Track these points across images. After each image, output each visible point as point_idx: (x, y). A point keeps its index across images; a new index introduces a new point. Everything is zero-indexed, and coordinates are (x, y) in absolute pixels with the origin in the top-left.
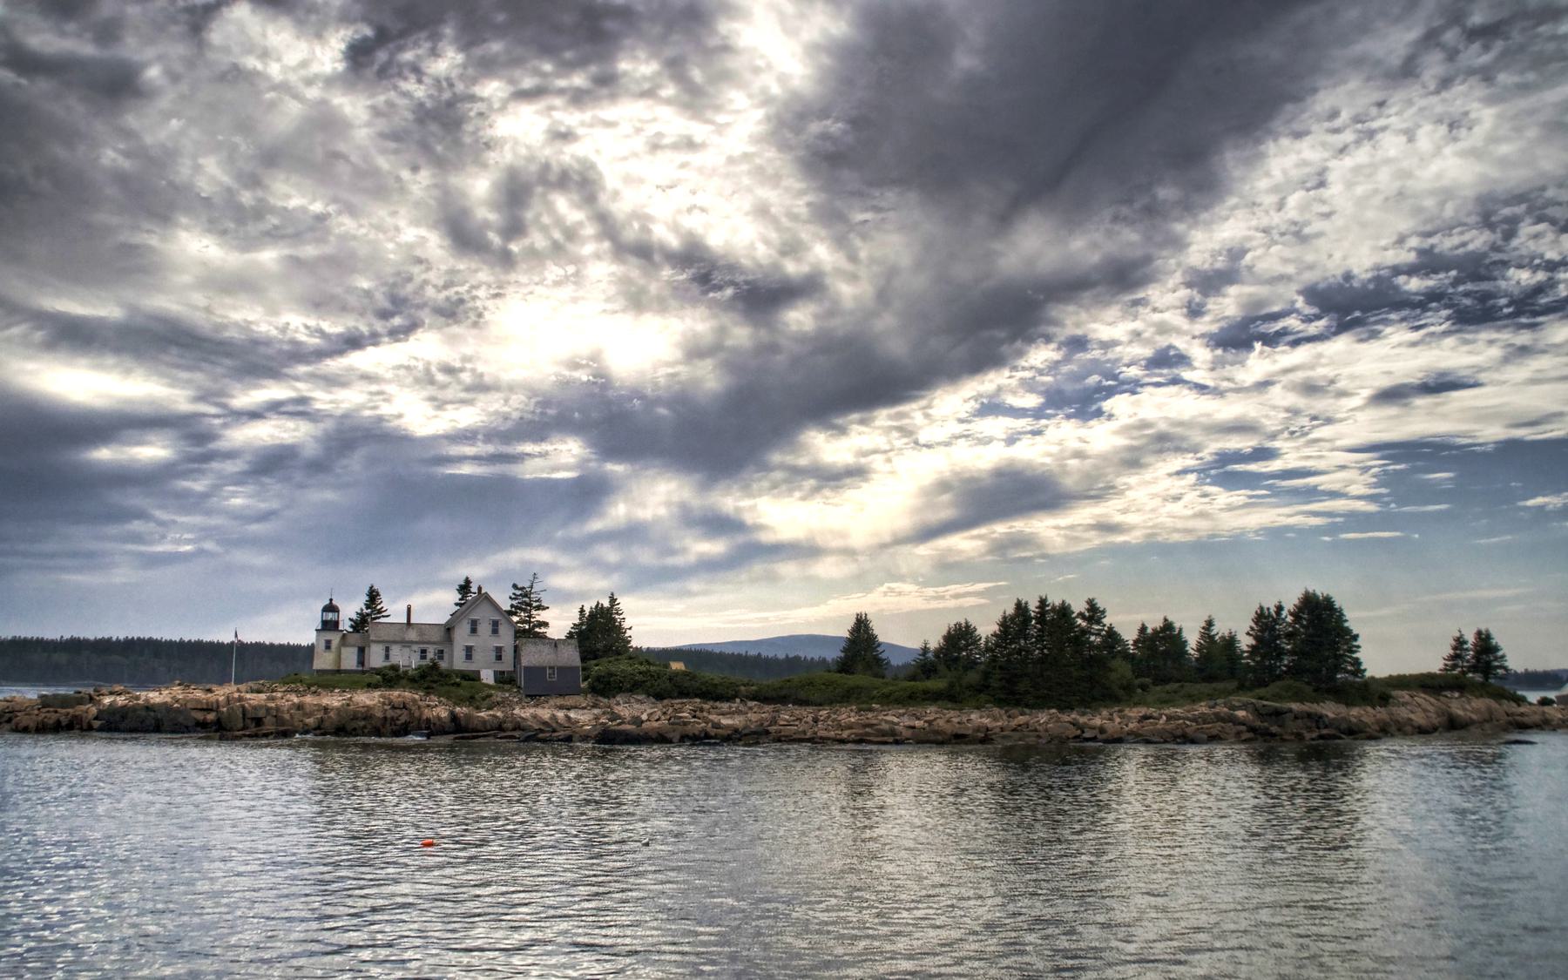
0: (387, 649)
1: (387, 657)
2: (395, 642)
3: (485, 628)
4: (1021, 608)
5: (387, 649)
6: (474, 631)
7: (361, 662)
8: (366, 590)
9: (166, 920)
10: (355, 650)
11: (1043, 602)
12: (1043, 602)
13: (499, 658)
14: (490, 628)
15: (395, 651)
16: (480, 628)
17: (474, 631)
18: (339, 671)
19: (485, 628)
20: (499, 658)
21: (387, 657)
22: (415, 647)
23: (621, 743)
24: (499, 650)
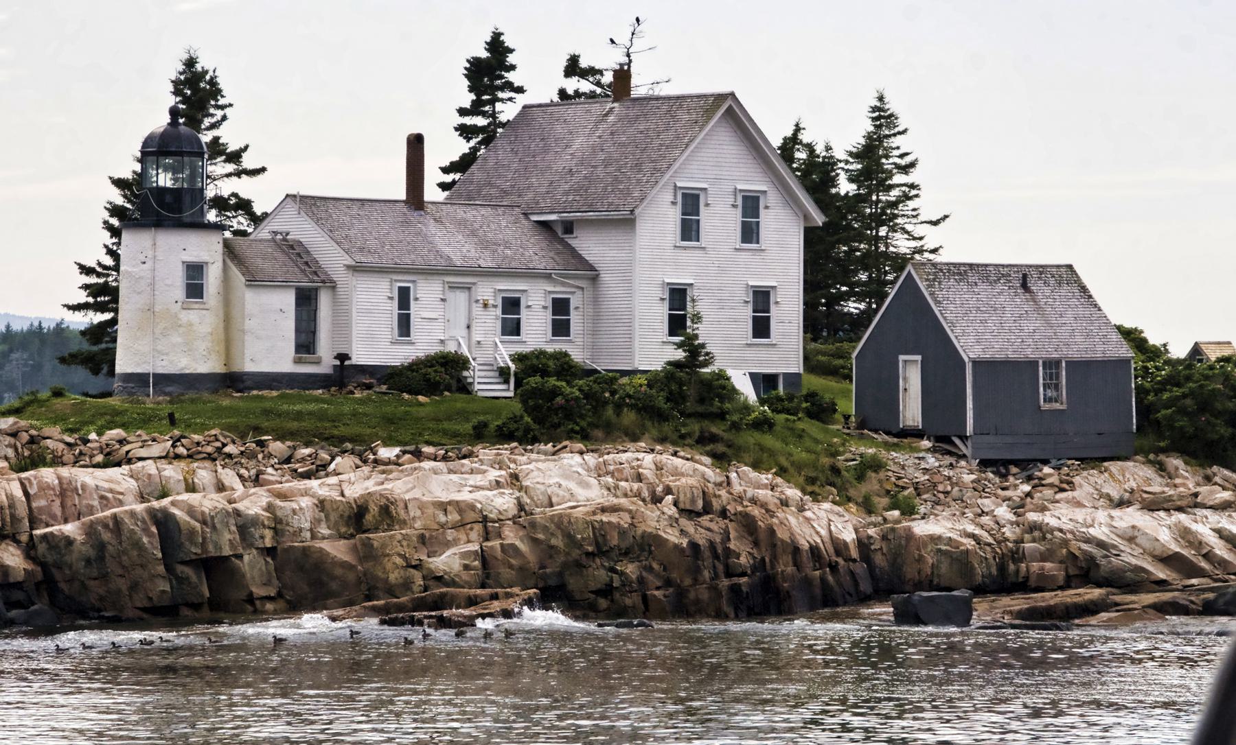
0: (404, 298)
1: (404, 326)
2: (429, 272)
3: (720, 220)
4: (1142, 332)
5: (404, 298)
6: (690, 230)
7: (306, 344)
8: (174, 68)
9: (1215, 629)
10: (288, 299)
11: (119, 183)
12: (119, 183)
13: (761, 328)
14: (734, 220)
15: (428, 296)
16: (707, 219)
17: (690, 230)
18: (232, 381)
19: (720, 220)
20: (761, 328)
21: (404, 326)
22: (487, 290)
23: (1080, 616)
24: (762, 299)
